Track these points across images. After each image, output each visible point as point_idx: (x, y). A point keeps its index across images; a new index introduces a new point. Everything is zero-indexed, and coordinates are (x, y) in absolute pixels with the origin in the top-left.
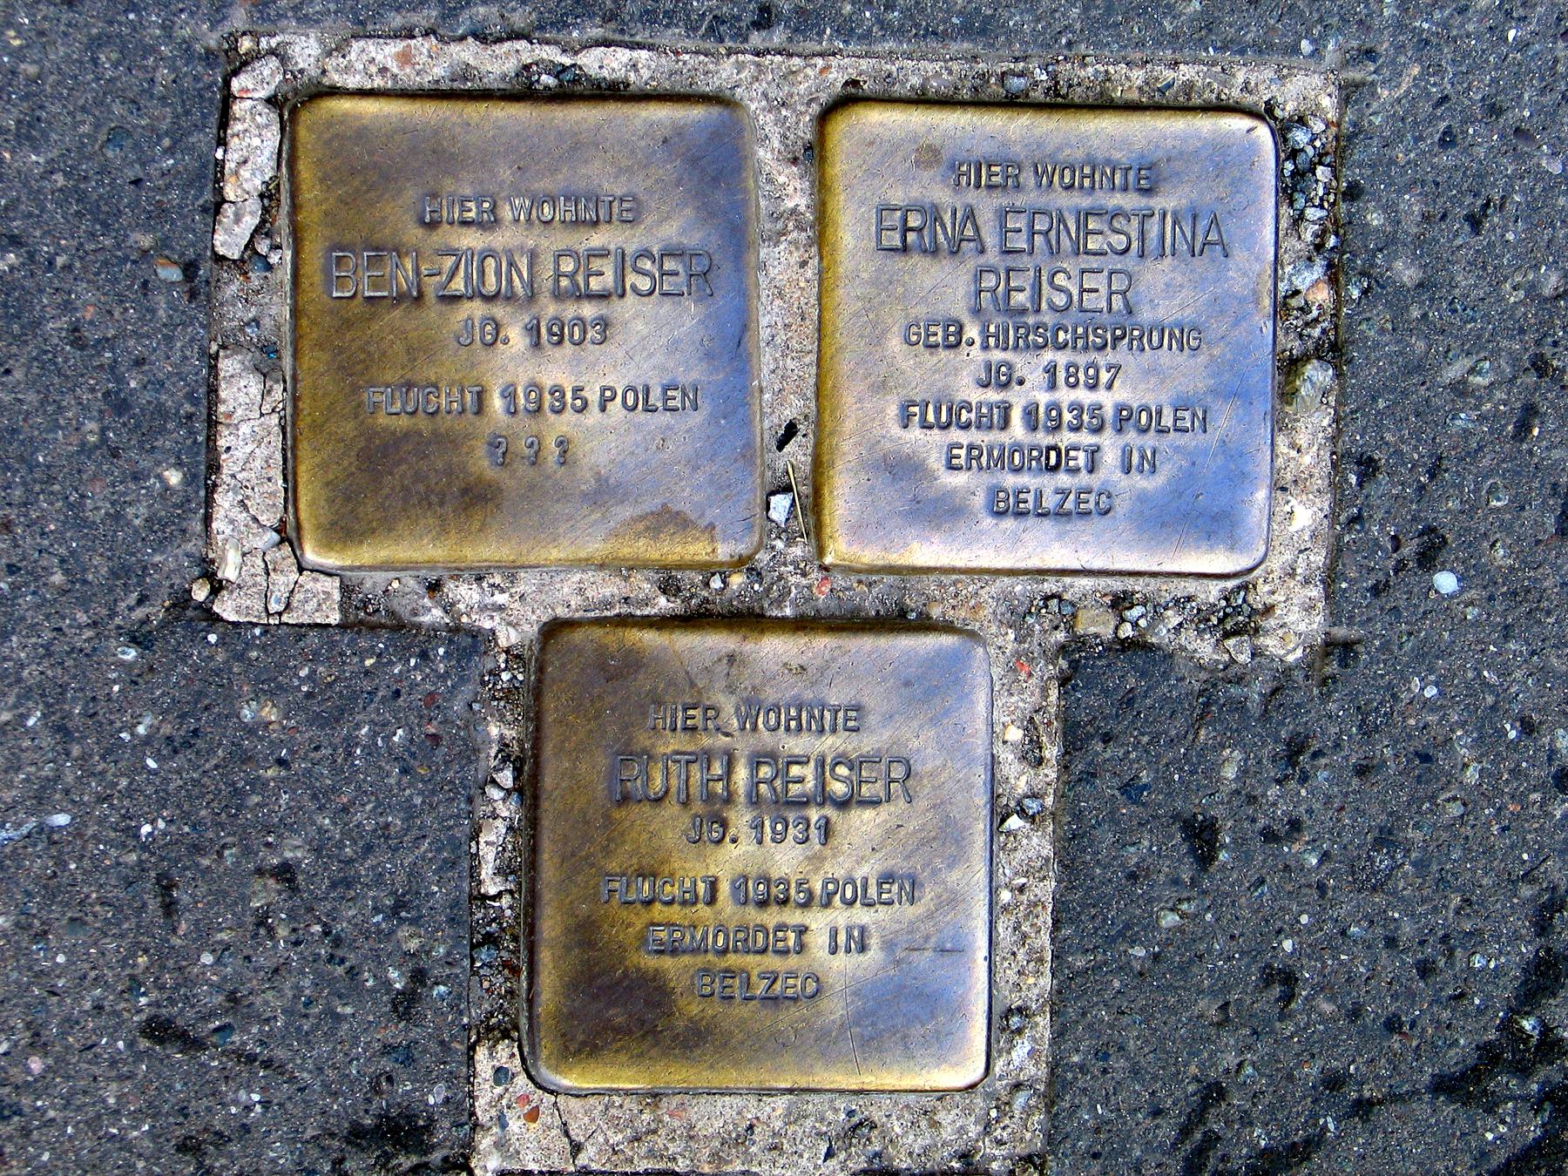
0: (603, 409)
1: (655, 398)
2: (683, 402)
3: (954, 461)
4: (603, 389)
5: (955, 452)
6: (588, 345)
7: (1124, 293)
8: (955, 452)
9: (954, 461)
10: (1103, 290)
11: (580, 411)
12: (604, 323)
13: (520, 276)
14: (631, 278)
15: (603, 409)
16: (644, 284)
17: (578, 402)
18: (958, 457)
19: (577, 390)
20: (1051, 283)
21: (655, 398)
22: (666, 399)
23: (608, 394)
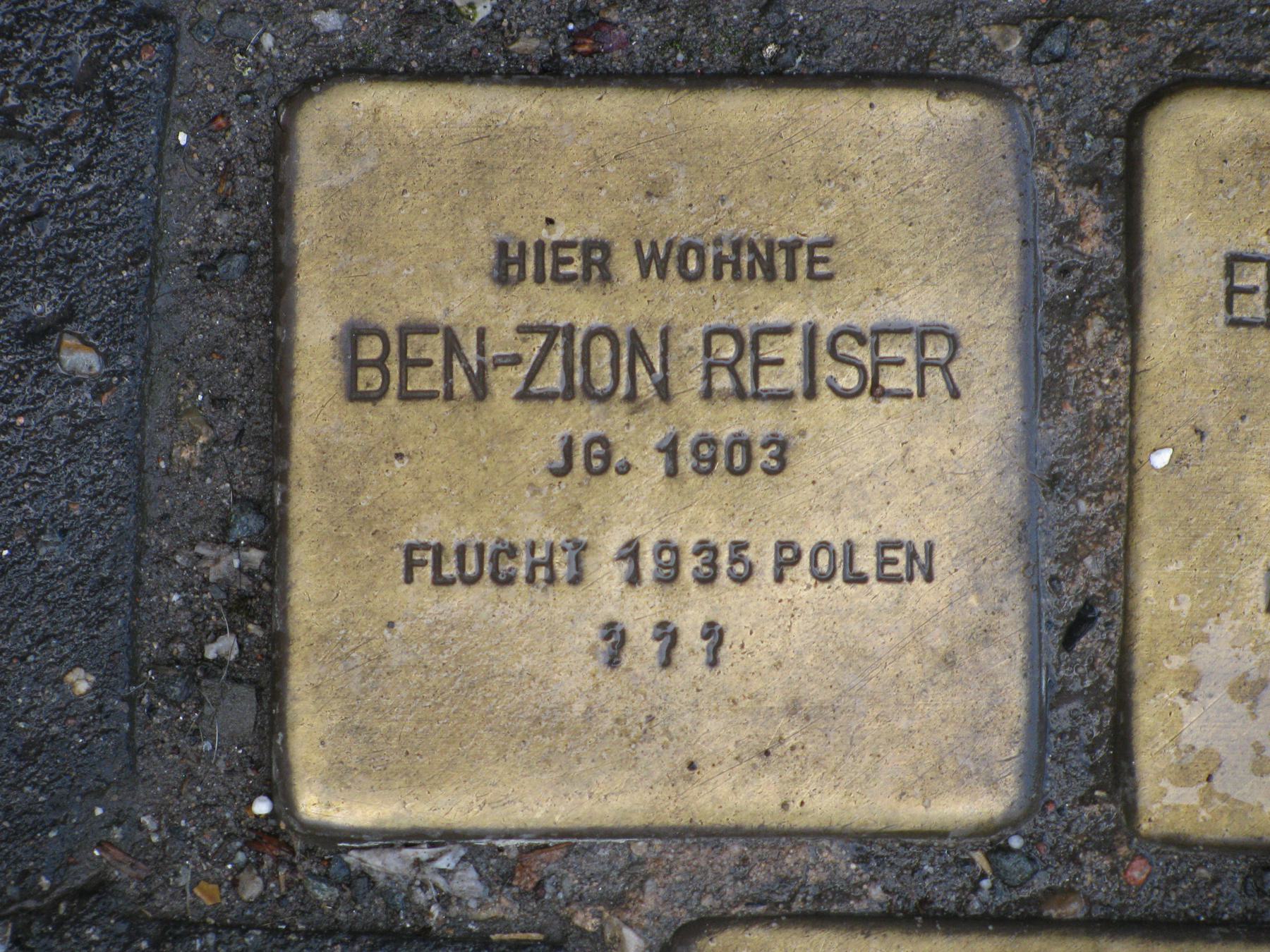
0: (779, 579)
1: (866, 562)
2: (910, 565)
3: (889, 569)
4: (782, 546)
5: (889, 554)
6: (756, 473)
7: (945, 367)
8: (889, 554)
9: (889, 569)
10: (911, 363)
11: (741, 580)
12: (781, 446)
13: (651, 371)
14: (826, 368)
15: (779, 579)
16: (849, 379)
17: (740, 568)
18: (894, 562)
19: (739, 547)
20: (832, 351)
21: (866, 562)
22: (883, 563)
23: (788, 554)
